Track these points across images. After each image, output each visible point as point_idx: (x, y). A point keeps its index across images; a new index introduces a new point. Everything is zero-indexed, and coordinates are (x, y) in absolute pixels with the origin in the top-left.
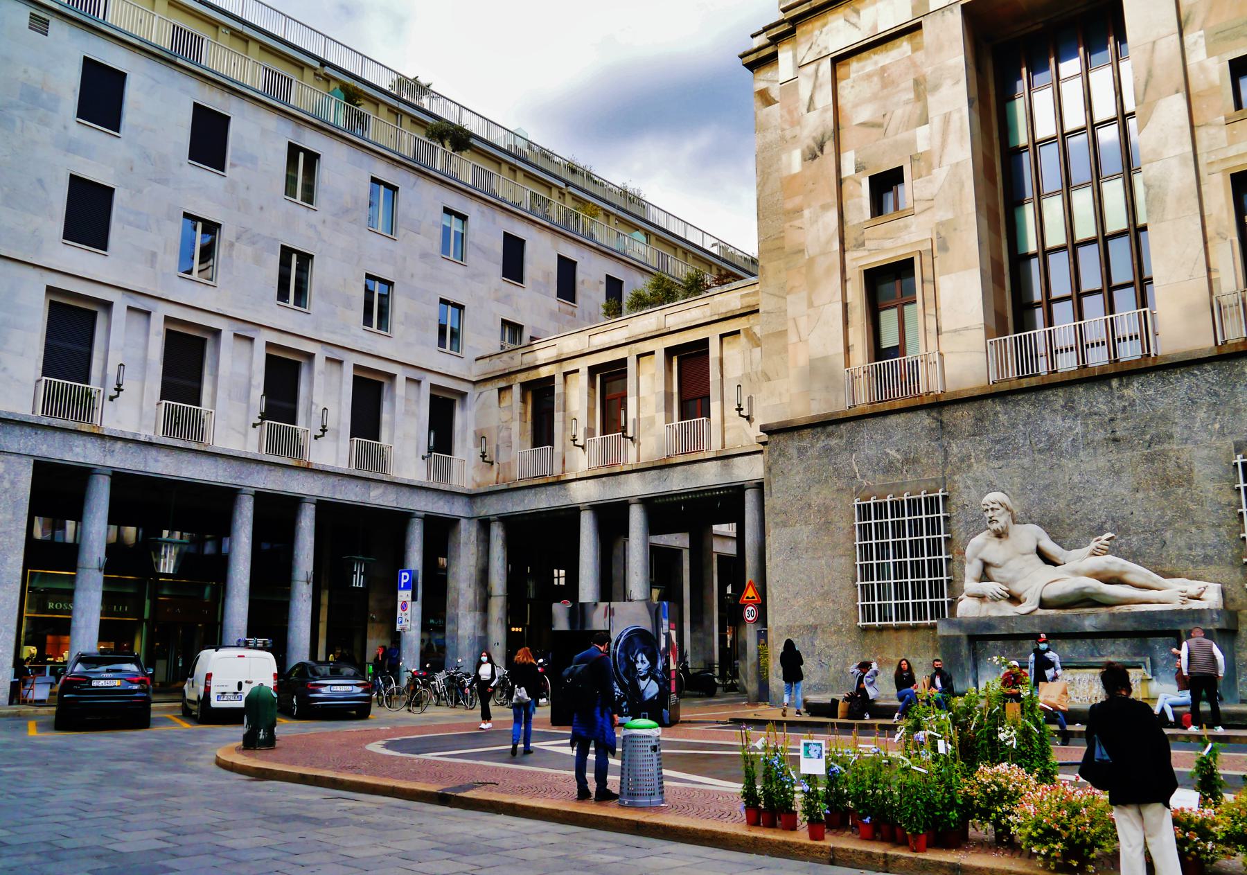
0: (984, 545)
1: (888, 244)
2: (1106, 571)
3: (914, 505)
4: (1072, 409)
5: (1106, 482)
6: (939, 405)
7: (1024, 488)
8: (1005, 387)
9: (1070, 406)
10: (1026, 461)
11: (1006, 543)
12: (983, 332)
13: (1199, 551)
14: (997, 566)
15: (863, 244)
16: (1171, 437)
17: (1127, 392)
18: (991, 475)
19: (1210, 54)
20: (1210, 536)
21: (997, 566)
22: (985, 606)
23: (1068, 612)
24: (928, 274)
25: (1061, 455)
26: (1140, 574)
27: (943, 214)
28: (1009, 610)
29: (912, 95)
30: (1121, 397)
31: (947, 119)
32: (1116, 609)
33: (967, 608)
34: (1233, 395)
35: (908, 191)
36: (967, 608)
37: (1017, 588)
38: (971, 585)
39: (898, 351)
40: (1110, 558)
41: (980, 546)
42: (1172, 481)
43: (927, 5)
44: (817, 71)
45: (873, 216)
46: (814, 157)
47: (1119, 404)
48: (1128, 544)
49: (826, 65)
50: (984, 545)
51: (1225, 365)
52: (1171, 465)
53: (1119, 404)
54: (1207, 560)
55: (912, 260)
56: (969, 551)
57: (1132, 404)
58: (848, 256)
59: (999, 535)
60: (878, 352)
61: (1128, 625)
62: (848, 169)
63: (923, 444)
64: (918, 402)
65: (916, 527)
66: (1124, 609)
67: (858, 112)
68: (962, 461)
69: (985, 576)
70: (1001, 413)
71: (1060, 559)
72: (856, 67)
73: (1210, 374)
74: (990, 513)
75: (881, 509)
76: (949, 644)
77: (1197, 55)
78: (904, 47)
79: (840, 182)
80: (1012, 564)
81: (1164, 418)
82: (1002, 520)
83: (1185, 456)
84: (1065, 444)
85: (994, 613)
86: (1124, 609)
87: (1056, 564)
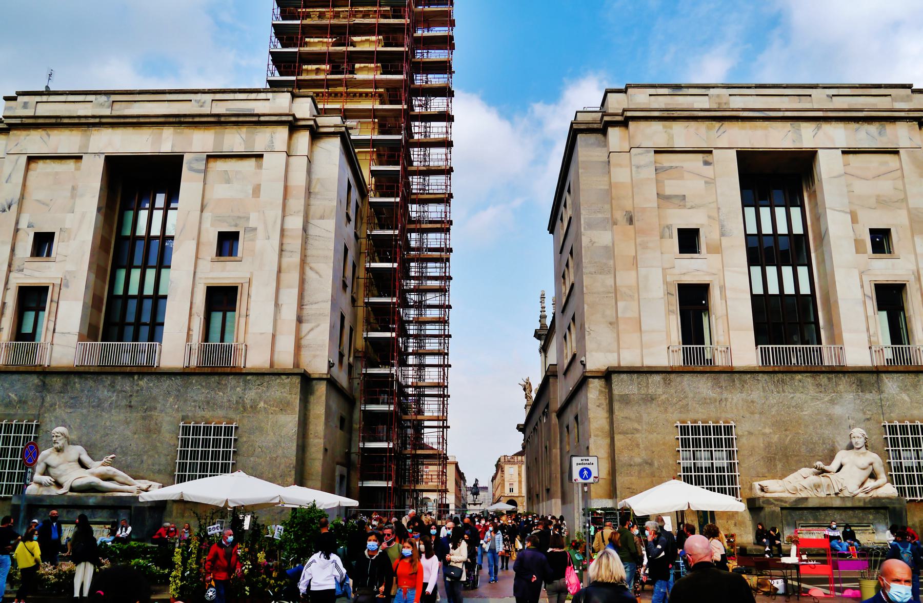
0: (49, 455)
1: (37, 274)
2: (106, 474)
3: (218, 430)
4: (113, 387)
5: (122, 427)
6: (46, 373)
7: (80, 425)
8: (81, 369)
9: (112, 385)
10: (85, 411)
11: (62, 455)
12: (77, 337)
13: (156, 467)
14: (54, 467)
15: (22, 270)
16: (156, 409)
17: (141, 383)
18: (65, 416)
19: (212, 225)
20: (163, 460)
21: (54, 467)
22: (41, 489)
23: (83, 494)
24: (55, 298)
25: (103, 410)
26: (123, 477)
27: (70, 267)
28: (55, 491)
29: (69, 194)
30: (138, 385)
31: (83, 215)
32: (107, 494)
33: (32, 489)
34: (186, 392)
35: (58, 246)
36: (32, 489)
37: (61, 480)
38: (37, 477)
39: (32, 337)
40: (109, 468)
41: (47, 455)
42: (151, 430)
43: (87, 147)
44: (17, 160)
45: (32, 255)
46: (4, 211)
47: (136, 388)
48: (126, 460)
49: (24, 159)
50: (49, 455)
51: (186, 378)
52: (153, 423)
53: (136, 388)
54: (159, 472)
55: (47, 288)
56: (40, 458)
57: (142, 389)
58: (12, 275)
59: (59, 450)
60: (19, 335)
61: (110, 503)
62: (23, 225)
63: (31, 394)
64: (33, 369)
65: (216, 443)
66: (110, 494)
67: (36, 192)
68: (51, 406)
69: (46, 473)
70: (77, 383)
71: (89, 466)
72: (40, 166)
73: (178, 381)
74: (54, 439)
75: (196, 430)
76: (16, 509)
77: (207, 225)
78: (71, 164)
79: (17, 230)
80: (62, 467)
81: (155, 399)
82: (61, 442)
83: (160, 419)
84: (106, 405)
85: (45, 493)
86: (110, 494)
87: (87, 468)
